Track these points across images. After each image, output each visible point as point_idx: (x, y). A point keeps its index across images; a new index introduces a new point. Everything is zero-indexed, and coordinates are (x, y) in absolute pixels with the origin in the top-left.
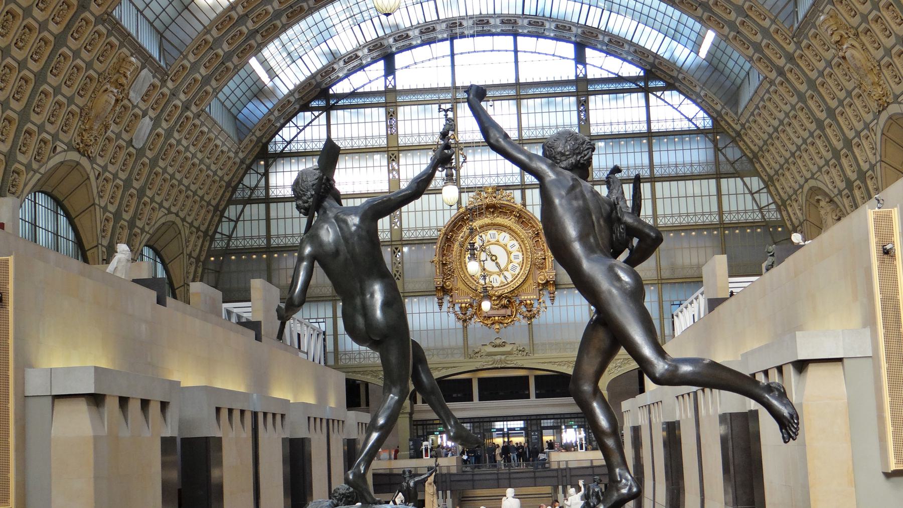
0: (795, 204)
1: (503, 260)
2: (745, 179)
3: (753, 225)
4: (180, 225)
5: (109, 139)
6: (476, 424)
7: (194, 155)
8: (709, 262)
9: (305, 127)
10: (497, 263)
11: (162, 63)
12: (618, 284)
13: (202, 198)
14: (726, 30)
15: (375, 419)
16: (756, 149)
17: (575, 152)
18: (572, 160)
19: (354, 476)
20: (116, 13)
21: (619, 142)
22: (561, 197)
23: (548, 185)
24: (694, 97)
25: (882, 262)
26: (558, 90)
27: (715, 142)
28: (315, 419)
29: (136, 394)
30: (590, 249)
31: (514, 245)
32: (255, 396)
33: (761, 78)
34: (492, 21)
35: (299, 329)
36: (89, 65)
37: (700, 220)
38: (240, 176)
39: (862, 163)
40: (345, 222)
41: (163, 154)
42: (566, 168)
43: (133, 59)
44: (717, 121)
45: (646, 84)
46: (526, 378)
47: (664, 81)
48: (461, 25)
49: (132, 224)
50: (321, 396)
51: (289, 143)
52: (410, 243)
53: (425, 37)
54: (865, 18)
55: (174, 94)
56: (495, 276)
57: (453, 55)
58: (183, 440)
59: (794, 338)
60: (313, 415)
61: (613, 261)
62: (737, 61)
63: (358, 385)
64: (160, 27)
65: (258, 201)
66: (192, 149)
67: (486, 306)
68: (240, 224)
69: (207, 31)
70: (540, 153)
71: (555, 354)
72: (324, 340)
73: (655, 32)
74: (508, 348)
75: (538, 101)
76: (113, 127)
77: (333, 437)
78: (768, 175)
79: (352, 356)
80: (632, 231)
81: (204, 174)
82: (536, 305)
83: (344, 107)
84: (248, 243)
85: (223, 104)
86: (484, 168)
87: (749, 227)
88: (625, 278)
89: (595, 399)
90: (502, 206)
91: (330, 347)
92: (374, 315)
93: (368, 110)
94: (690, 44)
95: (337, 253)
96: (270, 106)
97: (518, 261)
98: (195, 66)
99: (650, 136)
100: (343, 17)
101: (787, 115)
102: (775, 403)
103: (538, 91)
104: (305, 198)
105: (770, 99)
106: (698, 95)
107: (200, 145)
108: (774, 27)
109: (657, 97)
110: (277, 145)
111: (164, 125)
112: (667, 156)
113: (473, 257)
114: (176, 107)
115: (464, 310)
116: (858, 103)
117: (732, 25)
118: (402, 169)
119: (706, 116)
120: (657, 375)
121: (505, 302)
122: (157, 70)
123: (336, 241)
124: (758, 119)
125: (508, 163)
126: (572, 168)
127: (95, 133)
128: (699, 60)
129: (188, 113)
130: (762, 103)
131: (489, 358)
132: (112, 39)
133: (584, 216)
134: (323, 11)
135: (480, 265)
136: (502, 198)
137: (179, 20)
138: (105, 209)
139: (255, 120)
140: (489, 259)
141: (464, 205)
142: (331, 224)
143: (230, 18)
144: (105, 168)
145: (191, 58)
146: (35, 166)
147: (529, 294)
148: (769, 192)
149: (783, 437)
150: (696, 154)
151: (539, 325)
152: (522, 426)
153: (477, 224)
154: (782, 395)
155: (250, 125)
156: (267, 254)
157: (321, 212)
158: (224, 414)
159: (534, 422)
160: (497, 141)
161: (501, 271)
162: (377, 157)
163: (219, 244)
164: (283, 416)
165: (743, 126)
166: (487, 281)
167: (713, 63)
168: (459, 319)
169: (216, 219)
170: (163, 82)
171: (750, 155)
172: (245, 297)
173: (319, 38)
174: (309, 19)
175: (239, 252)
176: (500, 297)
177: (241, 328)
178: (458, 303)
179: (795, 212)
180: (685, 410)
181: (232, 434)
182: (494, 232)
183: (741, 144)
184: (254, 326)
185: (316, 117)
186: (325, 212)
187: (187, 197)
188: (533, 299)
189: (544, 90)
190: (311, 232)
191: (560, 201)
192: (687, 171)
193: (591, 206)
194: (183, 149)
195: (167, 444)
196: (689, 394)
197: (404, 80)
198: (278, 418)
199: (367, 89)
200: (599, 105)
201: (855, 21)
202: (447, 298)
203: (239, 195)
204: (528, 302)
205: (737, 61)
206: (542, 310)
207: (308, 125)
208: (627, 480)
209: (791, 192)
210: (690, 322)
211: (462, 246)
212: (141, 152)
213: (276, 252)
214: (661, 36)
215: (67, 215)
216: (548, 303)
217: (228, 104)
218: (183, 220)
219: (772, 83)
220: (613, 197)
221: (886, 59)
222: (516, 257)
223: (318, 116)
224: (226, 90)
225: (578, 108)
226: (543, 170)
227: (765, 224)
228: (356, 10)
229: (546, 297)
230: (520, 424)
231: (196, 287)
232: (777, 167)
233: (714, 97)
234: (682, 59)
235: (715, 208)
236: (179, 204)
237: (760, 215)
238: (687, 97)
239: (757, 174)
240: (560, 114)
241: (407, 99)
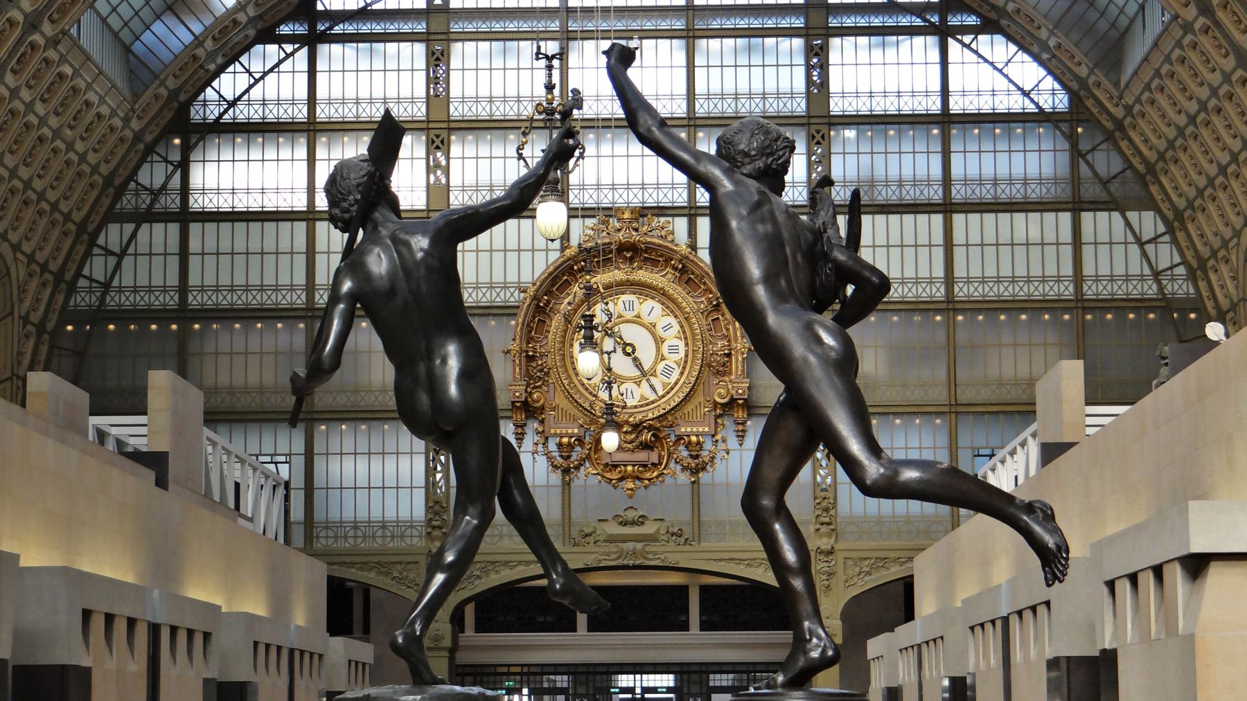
0: (1223, 268)
1: (646, 354)
2: (1129, 214)
3: (1140, 305)
6: (583, 678)
7: (43, 121)
8: (1049, 373)
9: (265, 74)
10: (635, 359)
12: (819, 350)
13: (55, 206)
15: (441, 552)
17: (763, 152)
18: (760, 164)
19: (405, 638)
21: (886, 132)
22: (741, 218)
23: (723, 201)
24: (1036, 49)
26: (770, 23)
27: (1073, 139)
28: (268, 646)
30: (779, 296)
32: (156, 593)
33: (1167, 18)
35: (237, 474)
37: (1037, 291)
38: (132, 165)
40: (407, 244)
42: (749, 176)
44: (1080, 99)
45: (943, 19)
46: (683, 590)
47: (978, 15)
50: (279, 601)
51: (232, 104)
56: (629, 386)
59: (1185, 512)
60: (264, 639)
61: (817, 317)
63: (350, 591)
65: (166, 217)
66: (40, 108)
67: (610, 440)
68: (127, 262)
70: (713, 151)
72: (287, 498)
74: (649, 529)
75: (729, 42)
77: (300, 684)
78: (1174, 207)
79: (341, 532)
81: (61, 158)
82: (708, 445)
83: (344, 39)
84: (143, 300)
85: (104, 20)
86: (616, 170)
87: (1132, 310)
88: (828, 340)
89: (778, 520)
90: (650, 248)
91: (297, 513)
92: (445, 391)
93: (392, 47)
95: (391, 292)
96: (198, 28)
97: (677, 357)
99: (946, 122)
101: (1214, 91)
102: (1037, 529)
103: (729, 24)
104: (345, 205)
105: (1182, 60)
106: (1044, 46)
107: (55, 101)
109: (964, 45)
110: (209, 107)
112: (976, 163)
113: (590, 343)
118: (455, 166)
119: (1057, 86)
120: (868, 482)
121: (647, 436)
123: (392, 274)
124: (1158, 96)
125: (665, 166)
126: (759, 176)
129: (36, 37)
130: (1166, 67)
131: (613, 547)
133: (772, 248)
135: (602, 360)
136: (651, 231)
139: (167, 57)
140: (619, 350)
141: (574, 241)
142: (385, 248)
147: (693, 424)
149: (1046, 578)
150: (1035, 162)
151: (712, 485)
152: (672, 684)
153: (601, 278)
154: (1048, 517)
155: (155, 66)
157: (369, 227)
158: (98, 623)
159: (695, 677)
160: (649, 130)
161: (644, 374)
163: (84, 299)
164: (207, 636)
165: (1129, 109)
166: (615, 392)
168: (556, 467)
169: (81, 249)
171: (1141, 168)
175: (123, 316)
176: (637, 427)
177: (130, 463)
178: (555, 435)
180: (986, 655)
181: (111, 665)
182: (632, 297)
183: (1124, 144)
184: (155, 462)
185: (288, 56)
186: (375, 228)
187: (26, 203)
188: (703, 434)
189: (742, 23)
190: (352, 258)
191: (738, 223)
192: (1017, 193)
193: (786, 234)
194: (21, 108)
196: (993, 622)
198: (198, 640)
200: (849, 56)
202: (533, 426)
203: (128, 202)
204: (694, 439)
206: (719, 456)
207: (271, 70)
208: (819, 638)
209: (1217, 243)
211: (568, 320)
213: (197, 320)
216: (733, 442)
217: (114, 22)
218: (16, 248)
219: (1187, 27)
220: (819, 222)
222: (673, 349)
223: (292, 54)
225: (808, 60)
226: (715, 177)
227: (1165, 304)
230: (667, 680)
231: (39, 381)
233: (1074, 50)
235: (1067, 269)
237: (1155, 287)
238: (1023, 47)
239: (1152, 205)
240: (771, 72)
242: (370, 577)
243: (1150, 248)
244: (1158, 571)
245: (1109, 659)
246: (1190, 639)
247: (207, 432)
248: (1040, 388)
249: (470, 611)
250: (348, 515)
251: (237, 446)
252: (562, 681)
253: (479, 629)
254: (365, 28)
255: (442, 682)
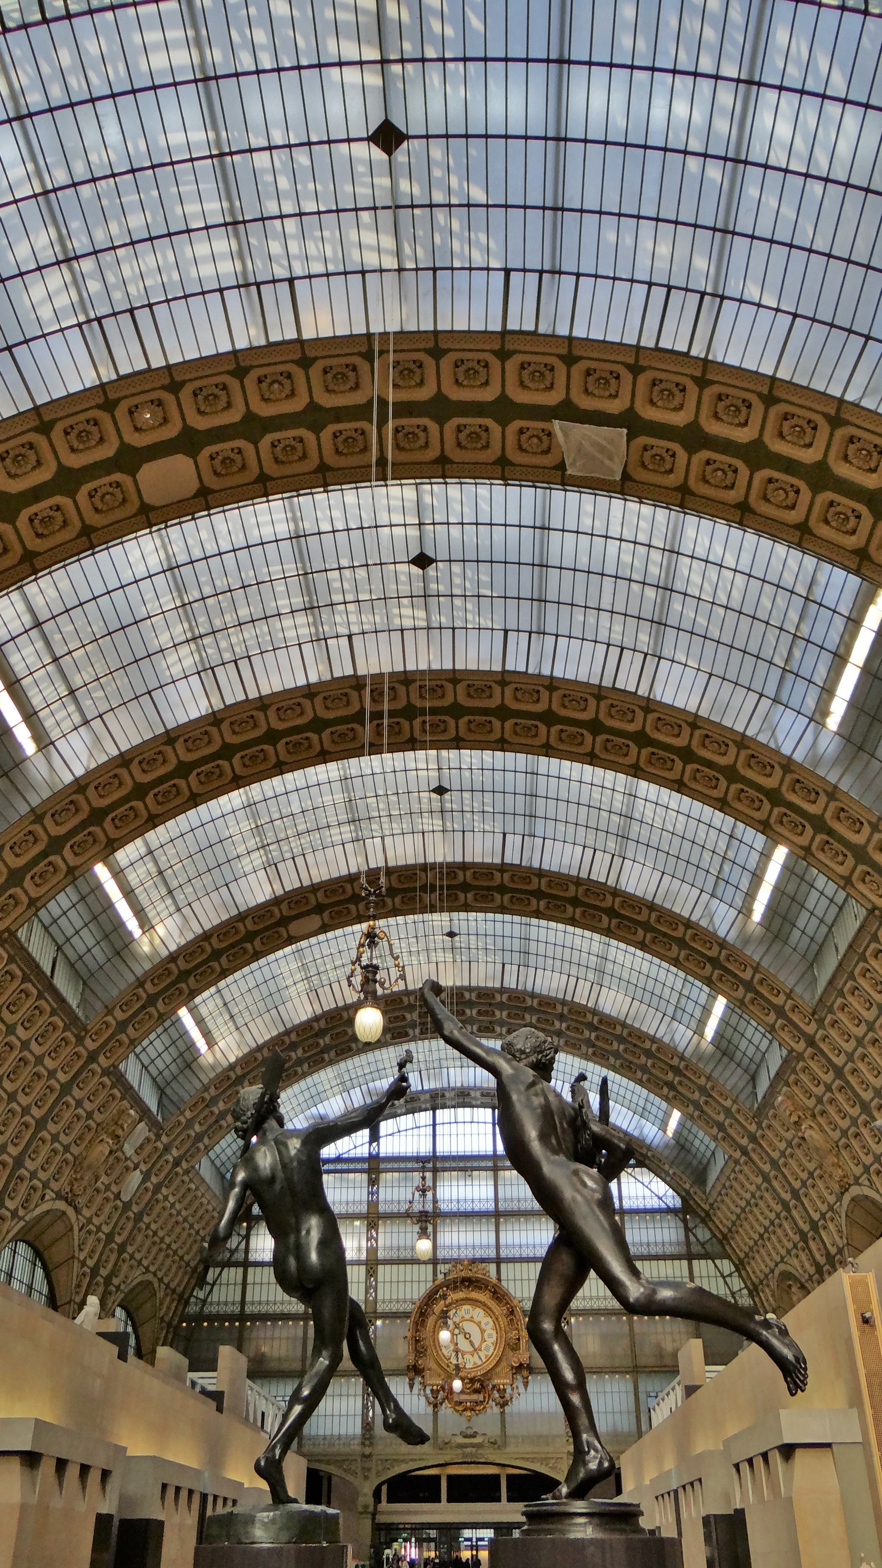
4: (156, 1285)
5: (98, 1191)
11: (159, 1118)
13: (182, 1258)
14: (691, 1109)
15: (298, 1390)
16: (725, 1230)
18: (533, 1058)
20: (122, 1067)
22: (519, 1092)
25: (862, 1332)
27: (685, 1221)
29: (76, 1456)
31: (488, 1322)
34: (472, 1093)
36: (90, 1115)
39: (829, 1246)
41: (148, 1208)
43: (132, 1112)
46: (497, 1477)
48: (443, 1096)
49: (108, 1281)
52: (384, 1316)
53: (409, 1106)
54: (820, 1100)
55: (167, 1149)
57: (434, 1125)
58: (123, 1522)
59: (777, 1418)
62: (703, 1141)
64: (162, 1084)
65: (236, 1264)
68: (216, 1288)
69: (206, 1089)
70: (499, 1048)
71: (529, 1448)
73: (624, 1110)
74: (478, 1440)
76: (104, 1179)
80: (600, 1142)
82: (509, 1390)
84: (223, 1309)
90: (478, 1280)
94: (658, 1122)
95: (272, 1180)
98: (190, 1123)
100: (334, 1083)
101: (753, 1196)
102: (775, 1342)
105: (736, 1179)
106: (667, 1173)
107: (180, 1195)
108: (735, 1107)
111: (154, 1180)
114: (167, 1162)
115: (435, 1393)
116: (820, 1183)
117: (697, 1105)
121: (477, 1385)
122: (154, 1124)
123: (273, 1169)
126: (535, 1066)
127: (85, 1183)
128: (666, 1139)
129: (178, 1169)
131: (459, 1451)
132: (115, 1091)
134: (315, 1076)
136: (477, 1272)
137: (181, 1078)
138: (83, 1264)
143: (229, 1078)
144: (89, 1221)
145: (188, 1114)
146: (21, 1213)
148: (740, 1276)
151: (511, 1414)
156: (241, 1324)
158: (171, 1492)
162: (357, 1223)
163: (193, 1309)
165: (711, 1205)
167: (681, 1143)
170: (158, 1137)
172: (211, 1365)
173: (310, 1102)
174: (302, 1083)
175: (211, 1318)
176: (472, 1380)
179: (767, 1296)
184: (217, 1397)
192: (659, 1250)
195: (103, 1521)
197: (388, 1147)
199: (352, 1154)
201: (811, 1103)
202: (418, 1379)
205: (703, 1141)
209: (762, 1277)
210: (667, 1413)
212: (127, 1206)
214: (631, 1113)
215: (45, 1267)
216: (522, 1389)
217: (218, 1163)
218: (160, 1280)
219: (736, 1162)
221: (844, 1140)
222: (490, 1336)
224: (217, 1148)
228: (347, 1078)
229: (519, 1382)
230: (489, 1533)
231: (164, 1352)
232: (747, 1249)
234: (651, 1136)
236: (158, 1262)
238: (657, 1175)
239: (726, 1256)
241: (389, 1166)
242: (331, 1469)
243: (728, 1279)
244: (765, 1456)
245: (740, 1514)
246: (790, 1500)
247: (248, 1382)
248: (680, 1355)
249: (384, 1488)
250: (321, 1432)
251: (264, 1391)
252: (433, 1533)
253: (389, 1501)
254: (339, 1166)
255: (295, 1501)
